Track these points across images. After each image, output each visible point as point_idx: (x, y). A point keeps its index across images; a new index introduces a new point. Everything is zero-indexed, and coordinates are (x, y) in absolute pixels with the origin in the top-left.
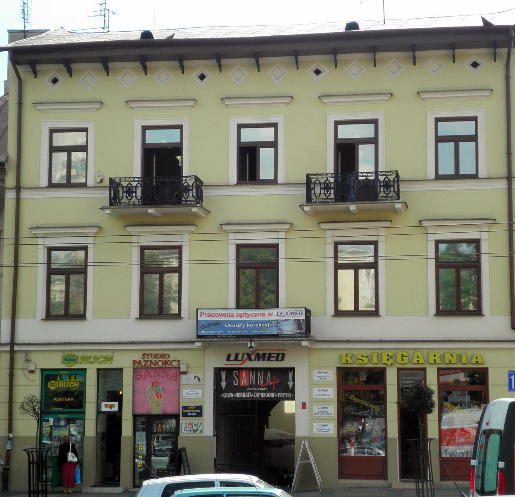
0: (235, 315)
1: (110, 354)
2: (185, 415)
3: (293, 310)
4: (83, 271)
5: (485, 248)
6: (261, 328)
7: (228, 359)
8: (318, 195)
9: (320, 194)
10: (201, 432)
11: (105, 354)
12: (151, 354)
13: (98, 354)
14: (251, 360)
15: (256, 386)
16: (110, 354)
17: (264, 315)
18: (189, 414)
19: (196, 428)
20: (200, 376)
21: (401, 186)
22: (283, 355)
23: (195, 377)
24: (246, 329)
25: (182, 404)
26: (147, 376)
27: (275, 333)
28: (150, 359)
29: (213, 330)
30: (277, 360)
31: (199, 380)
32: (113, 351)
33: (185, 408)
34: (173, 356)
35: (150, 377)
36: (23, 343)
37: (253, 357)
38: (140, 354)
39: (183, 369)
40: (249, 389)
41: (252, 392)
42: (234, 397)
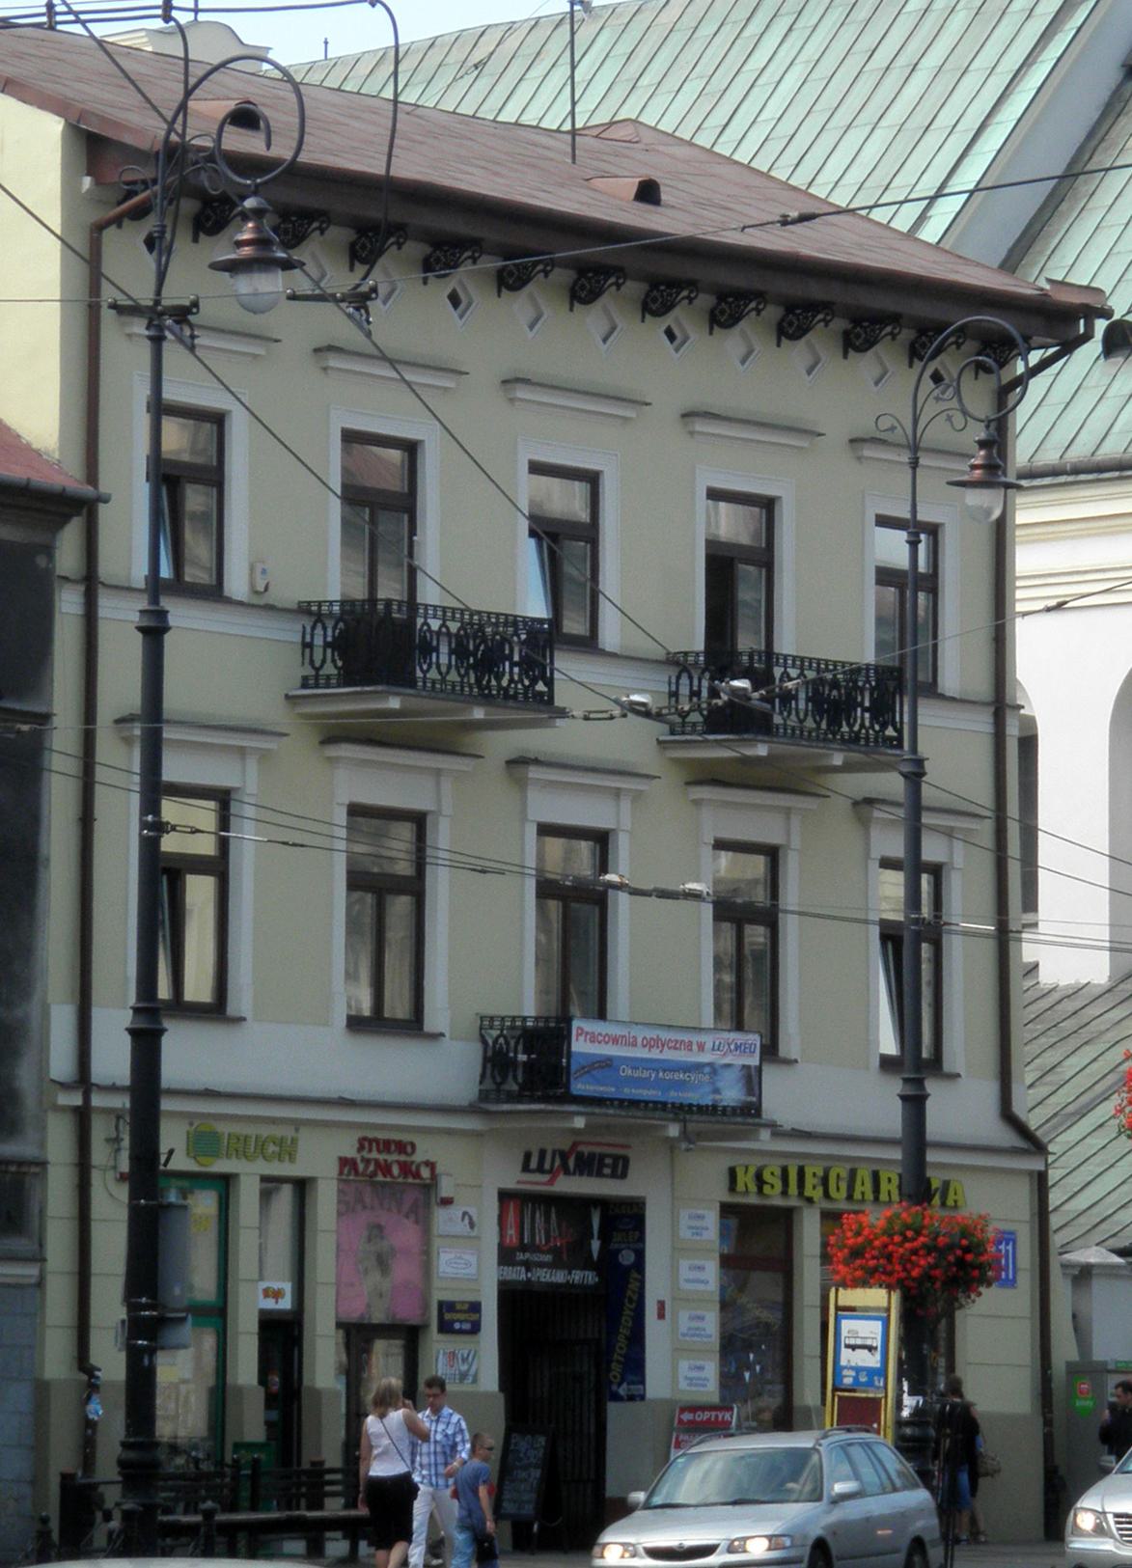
0: (709, 1046)
1: (288, 1132)
2: (445, 1328)
3: (651, 1034)
4: (415, 887)
5: (442, 837)
6: (680, 1085)
7: (526, 1168)
8: (317, 664)
9: (324, 661)
10: (475, 1381)
11: (278, 1131)
12: (377, 1141)
13: (265, 1131)
14: (567, 1172)
15: (533, 1248)
16: (288, 1132)
17: (689, 1046)
18: (457, 1326)
19: (464, 1368)
20: (472, 1211)
21: (920, 711)
22: (626, 1160)
23: (465, 1214)
24: (658, 1084)
25: (438, 1295)
26: (359, 1207)
27: (708, 1101)
28: (374, 1155)
29: (598, 1082)
30: (614, 1175)
31: (472, 1225)
32: (297, 1124)
33: (445, 1307)
34: (425, 1150)
35: (365, 1207)
36: (335, 1096)
37: (571, 1163)
38: (364, 1143)
39: (446, 1189)
40: (520, 1256)
41: (528, 1265)
42: (529, 1280)
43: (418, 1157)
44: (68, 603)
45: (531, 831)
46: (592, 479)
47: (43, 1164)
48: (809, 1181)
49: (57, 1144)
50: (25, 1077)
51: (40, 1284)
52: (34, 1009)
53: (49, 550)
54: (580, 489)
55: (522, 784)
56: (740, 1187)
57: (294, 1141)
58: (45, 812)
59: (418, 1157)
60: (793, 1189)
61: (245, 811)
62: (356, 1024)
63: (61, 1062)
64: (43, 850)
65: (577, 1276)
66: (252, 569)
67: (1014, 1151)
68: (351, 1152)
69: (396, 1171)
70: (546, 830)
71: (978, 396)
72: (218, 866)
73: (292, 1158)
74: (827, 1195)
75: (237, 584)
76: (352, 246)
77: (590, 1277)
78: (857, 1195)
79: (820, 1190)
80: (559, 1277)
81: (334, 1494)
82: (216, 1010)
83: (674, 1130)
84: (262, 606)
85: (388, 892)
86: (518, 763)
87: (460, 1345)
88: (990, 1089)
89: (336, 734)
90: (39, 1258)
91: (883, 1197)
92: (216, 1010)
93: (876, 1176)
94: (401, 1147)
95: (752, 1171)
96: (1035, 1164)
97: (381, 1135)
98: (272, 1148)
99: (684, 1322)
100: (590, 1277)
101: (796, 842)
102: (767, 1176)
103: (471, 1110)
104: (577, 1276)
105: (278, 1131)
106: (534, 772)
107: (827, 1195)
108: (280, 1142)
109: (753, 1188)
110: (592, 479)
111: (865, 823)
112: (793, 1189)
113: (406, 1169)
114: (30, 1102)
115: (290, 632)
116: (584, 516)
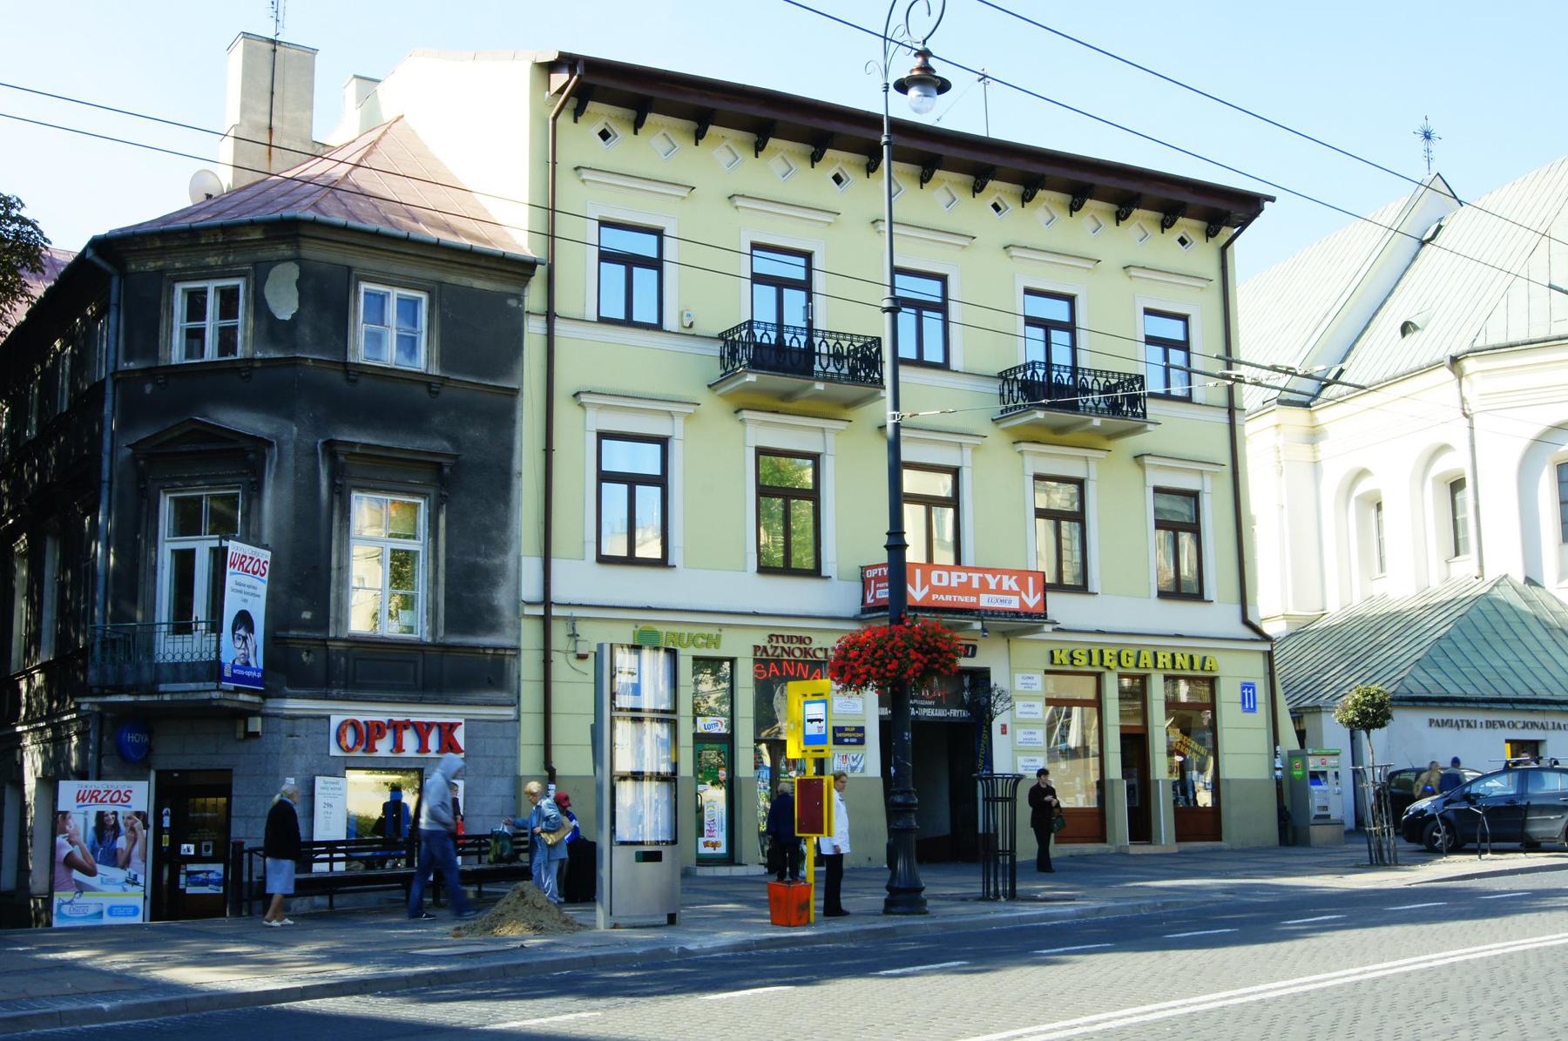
1: (714, 631)
10: (863, 770)
11: (706, 631)
13: (695, 631)
16: (714, 631)
22: (975, 648)
32: (721, 626)
43: (814, 645)
44: (534, 329)
45: (1150, 492)
46: (1185, 318)
47: (517, 649)
48: (1107, 657)
49: (529, 636)
50: (502, 598)
51: (518, 720)
52: (510, 560)
53: (520, 298)
54: (1180, 324)
55: (1142, 466)
56: (1057, 661)
57: (718, 637)
58: (517, 445)
59: (814, 645)
60: (1096, 660)
61: (676, 449)
62: (1163, 595)
63: (530, 588)
64: (516, 468)
65: (954, 713)
66: (682, 314)
67: (1252, 640)
68: (763, 642)
69: (797, 653)
70: (1157, 490)
71: (1202, 255)
72: (814, 495)
73: (717, 646)
74: (1120, 664)
75: (670, 322)
76: (1117, 213)
77: (964, 714)
78: (1141, 665)
79: (1115, 663)
80: (941, 713)
81: (331, 846)
82: (1082, 588)
83: (977, 625)
84: (688, 332)
85: (783, 492)
86: (1138, 458)
87: (853, 751)
88: (1236, 610)
89: (743, 405)
90: (516, 703)
91: (1160, 665)
92: (1082, 588)
93: (1101, 652)
94: (801, 640)
95: (1065, 652)
96: (1266, 647)
97: (798, 634)
98: (700, 640)
99: (1020, 735)
100: (964, 714)
101: (1093, 476)
102: (1076, 655)
103: (855, 619)
104: (954, 713)
105: (706, 631)
106: (1147, 460)
107: (1120, 664)
108: (708, 637)
109: (1066, 661)
110: (1070, 299)
111: (1142, 466)
112: (1096, 660)
113: (805, 652)
114: (508, 614)
115: (994, 387)
116: (654, 255)
